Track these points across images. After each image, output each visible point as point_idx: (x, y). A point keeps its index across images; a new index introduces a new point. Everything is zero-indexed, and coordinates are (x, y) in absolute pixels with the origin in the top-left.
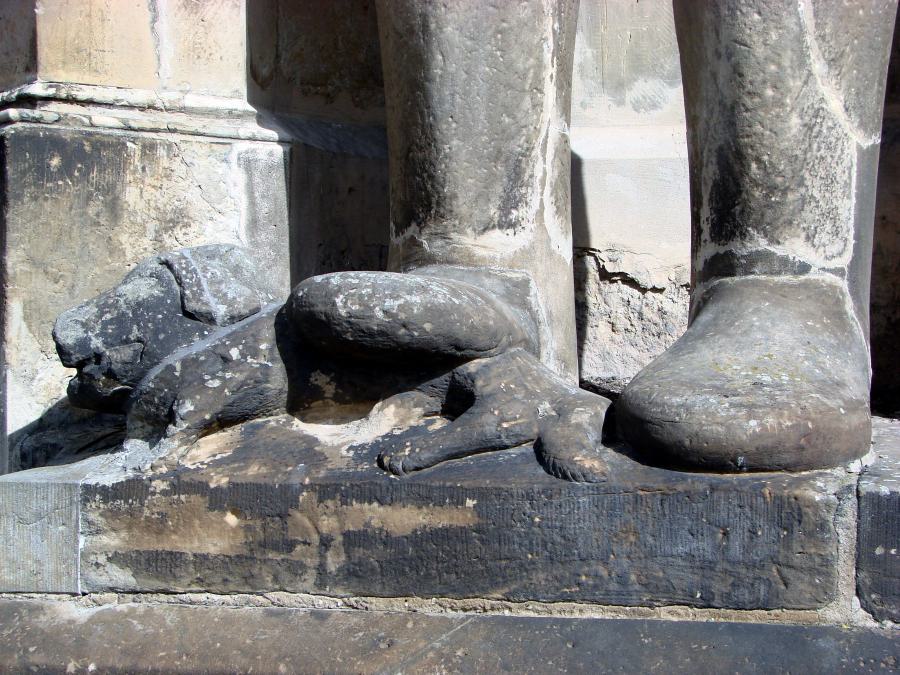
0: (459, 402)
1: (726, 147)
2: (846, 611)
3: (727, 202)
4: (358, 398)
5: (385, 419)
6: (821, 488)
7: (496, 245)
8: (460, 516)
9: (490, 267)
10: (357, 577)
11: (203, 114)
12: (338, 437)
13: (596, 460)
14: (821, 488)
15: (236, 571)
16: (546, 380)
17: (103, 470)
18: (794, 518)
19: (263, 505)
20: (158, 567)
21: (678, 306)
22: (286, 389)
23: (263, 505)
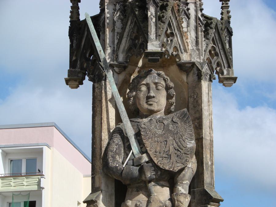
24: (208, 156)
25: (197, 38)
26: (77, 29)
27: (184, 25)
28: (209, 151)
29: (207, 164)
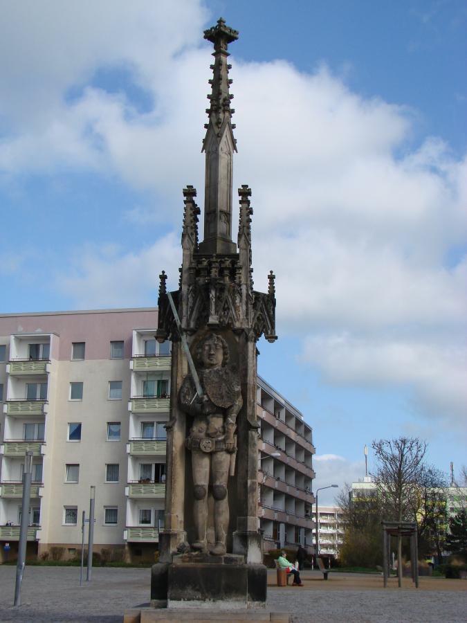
0: (201, 551)
1: (37, 524)
2: (223, 563)
3: (218, 539)
4: (195, 551)
5: (196, 553)
6: (222, 557)
7: (202, 541)
8: (201, 558)
9: (203, 542)
10: (195, 562)
11: (34, 616)
12: (194, 553)
13: (209, 555)
14: (222, 557)
15: (188, 562)
16: (206, 550)
17: (180, 555)
18: (221, 558)
19: (190, 557)
20: (183, 561)
21: (214, 545)
22: (183, 520)
23: (190, 557)
24: (251, 396)
25: (247, 310)
26: (163, 298)
27: (238, 301)
28: (251, 393)
29: (250, 401)
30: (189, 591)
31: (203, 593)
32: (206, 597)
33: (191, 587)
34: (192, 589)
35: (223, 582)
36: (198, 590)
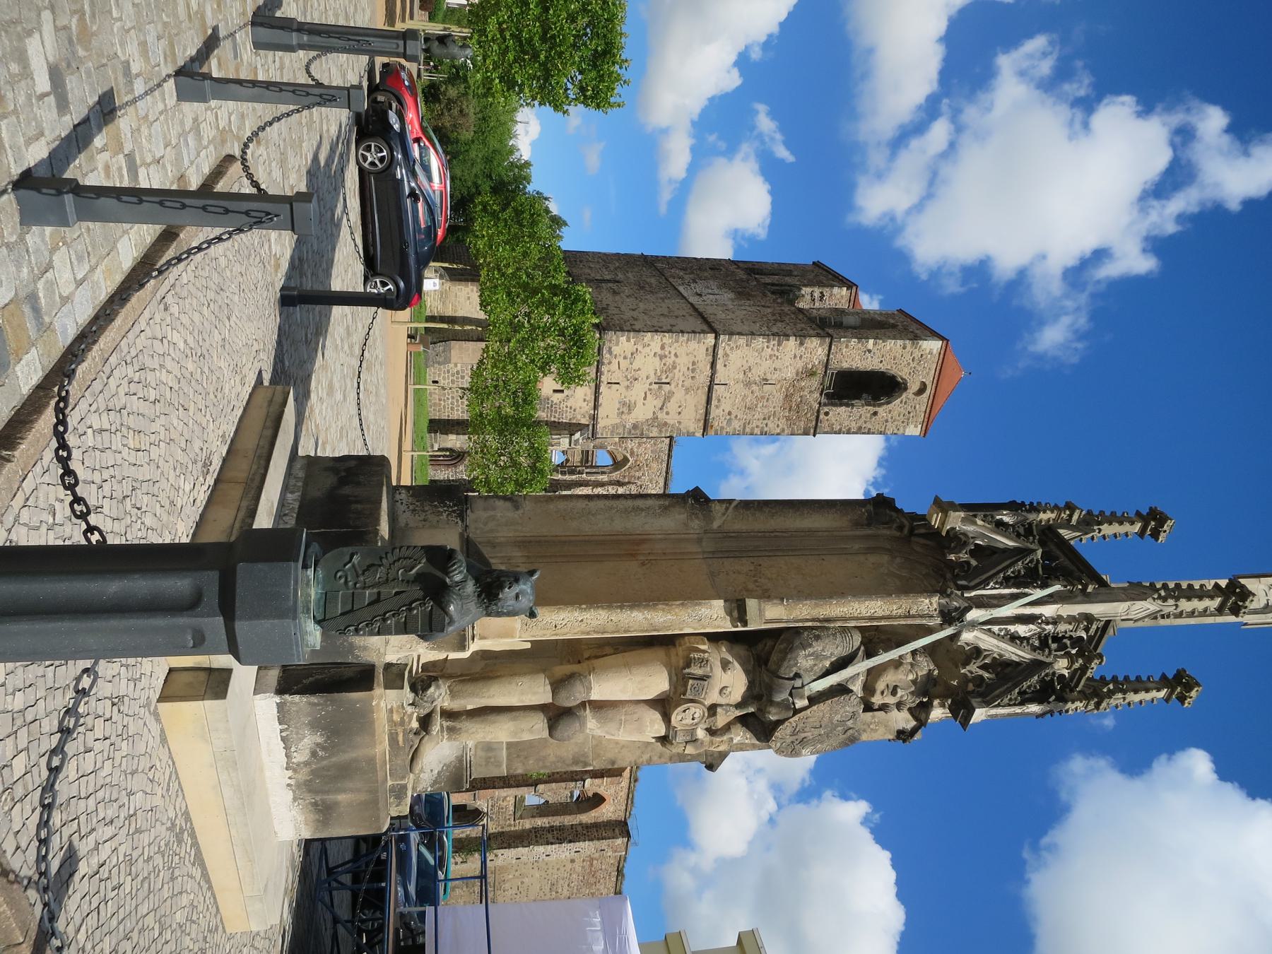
30: (308, 741)
31: (306, 764)
32: (295, 771)
33: (319, 740)
34: (318, 745)
35: (341, 797)
36: (314, 754)
